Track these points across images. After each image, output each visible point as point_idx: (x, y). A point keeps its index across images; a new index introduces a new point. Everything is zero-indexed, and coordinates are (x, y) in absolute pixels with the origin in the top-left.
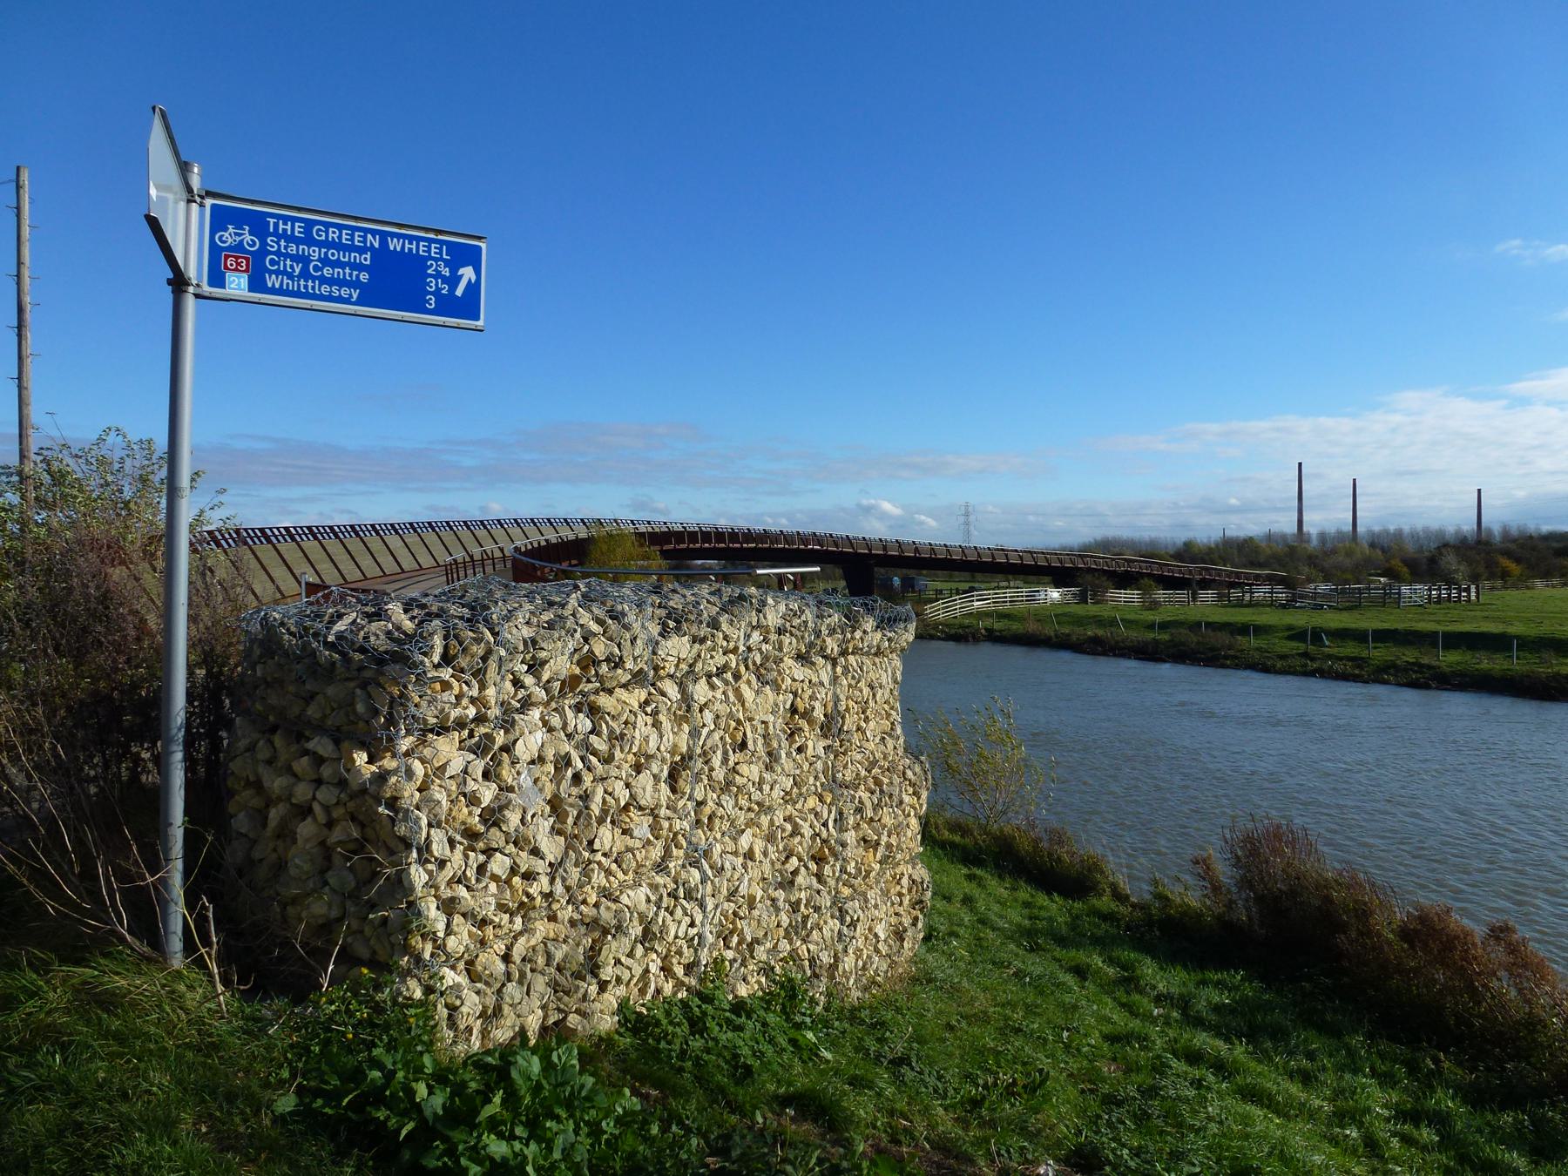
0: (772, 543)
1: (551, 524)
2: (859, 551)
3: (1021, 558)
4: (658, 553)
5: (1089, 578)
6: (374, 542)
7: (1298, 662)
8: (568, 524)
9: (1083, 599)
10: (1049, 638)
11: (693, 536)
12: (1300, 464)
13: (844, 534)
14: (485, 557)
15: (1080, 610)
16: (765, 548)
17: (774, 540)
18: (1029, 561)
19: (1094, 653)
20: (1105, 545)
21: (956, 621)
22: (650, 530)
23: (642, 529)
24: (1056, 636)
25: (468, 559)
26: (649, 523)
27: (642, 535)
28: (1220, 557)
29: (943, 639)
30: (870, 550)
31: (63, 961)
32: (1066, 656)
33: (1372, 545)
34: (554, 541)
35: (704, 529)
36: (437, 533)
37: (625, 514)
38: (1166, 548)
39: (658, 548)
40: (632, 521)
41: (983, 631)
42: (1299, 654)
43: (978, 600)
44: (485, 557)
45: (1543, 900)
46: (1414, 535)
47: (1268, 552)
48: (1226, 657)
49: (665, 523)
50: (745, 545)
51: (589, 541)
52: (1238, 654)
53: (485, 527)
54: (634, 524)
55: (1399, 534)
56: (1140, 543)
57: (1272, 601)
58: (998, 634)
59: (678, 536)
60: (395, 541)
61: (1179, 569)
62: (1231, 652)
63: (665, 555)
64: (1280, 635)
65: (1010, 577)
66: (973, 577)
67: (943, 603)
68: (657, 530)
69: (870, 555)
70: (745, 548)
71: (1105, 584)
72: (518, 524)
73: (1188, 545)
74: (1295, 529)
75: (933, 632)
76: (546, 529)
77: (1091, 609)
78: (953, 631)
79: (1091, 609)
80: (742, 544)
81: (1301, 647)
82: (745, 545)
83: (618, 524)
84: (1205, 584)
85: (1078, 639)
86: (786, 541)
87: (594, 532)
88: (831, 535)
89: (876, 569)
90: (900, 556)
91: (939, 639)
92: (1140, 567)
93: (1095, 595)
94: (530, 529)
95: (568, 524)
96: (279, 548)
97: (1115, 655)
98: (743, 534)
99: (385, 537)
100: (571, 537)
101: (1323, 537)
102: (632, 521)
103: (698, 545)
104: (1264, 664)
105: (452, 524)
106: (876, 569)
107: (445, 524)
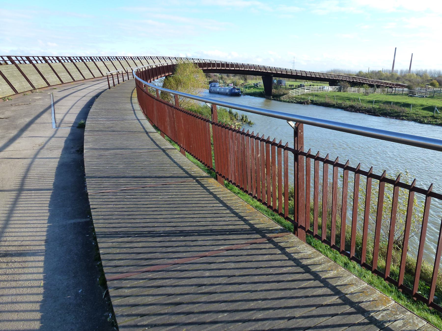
0: (245, 68)
2: (278, 72)
3: (306, 74)
5: (342, 83)
6: (91, 64)
7: (430, 119)
8: (170, 59)
9: (340, 90)
10: (334, 105)
12: (396, 48)
14: (118, 73)
15: (339, 94)
16: (247, 70)
17: (245, 67)
18: (304, 75)
19: (351, 111)
20: (334, 71)
21: (299, 97)
22: (199, 62)
23: (196, 62)
24: (337, 104)
25: (124, 72)
28: (370, 77)
29: (296, 103)
30: (282, 72)
32: (339, 111)
33: (417, 74)
36: (119, 61)
37: (190, 56)
38: (353, 72)
39: (202, 69)
40: (193, 59)
41: (310, 101)
42: (430, 116)
43: (306, 90)
46: (431, 72)
47: (385, 75)
48: (403, 116)
49: (204, 60)
50: (236, 69)
52: (407, 115)
53: (139, 59)
54: (193, 60)
55: (426, 71)
56: (345, 71)
57: (402, 93)
58: (315, 102)
59: (209, 64)
60: (100, 64)
61: (370, 80)
62: (404, 114)
64: (419, 108)
65: (308, 81)
66: (296, 80)
67: (295, 90)
68: (201, 62)
69: (272, 73)
70: (241, 70)
71: (348, 85)
73: (360, 72)
74: (391, 69)
75: (292, 100)
76: (150, 61)
77: (342, 94)
78: (299, 101)
79: (342, 94)
81: (431, 113)
82: (231, 68)
83: (193, 60)
84: (378, 86)
85: (345, 106)
86: (271, 70)
87: (179, 61)
88: (269, 67)
90: (286, 74)
91: (295, 103)
92: (343, 78)
93: (344, 89)
94: (144, 61)
95: (170, 59)
97: (360, 112)
98: (235, 65)
99: (135, 61)
100: (166, 65)
101: (402, 72)
104: (420, 120)
106: (273, 78)
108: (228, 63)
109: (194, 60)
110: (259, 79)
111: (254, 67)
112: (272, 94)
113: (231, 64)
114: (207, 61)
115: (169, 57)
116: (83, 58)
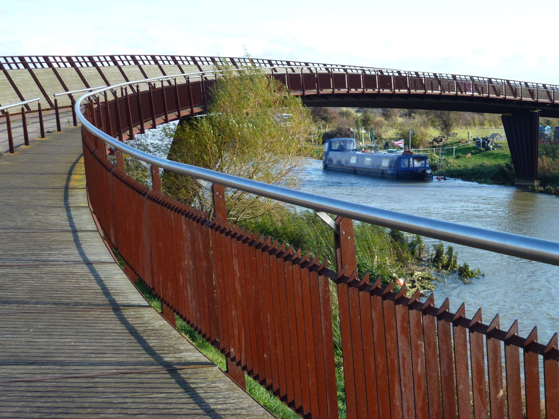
0: (443, 90)
1: (176, 62)
4: (299, 100)
11: (339, 80)
13: (524, 79)
14: (26, 110)
22: (290, 71)
23: (281, 71)
26: (288, 63)
27: (280, 77)
31: (355, 262)
34: (158, 85)
35: (368, 73)
39: (299, 93)
40: (270, 62)
44: (26, 110)
45: (112, 350)
49: (307, 64)
50: (413, 91)
51: (206, 84)
54: (272, 65)
63: (307, 101)
68: (298, 72)
69: (537, 104)
72: (136, 62)
80: (409, 89)
89: (541, 120)
96: (103, 71)
98: (411, 78)
100: (181, 81)
102: (270, 62)
103: (360, 90)
105: (51, 59)
107: (42, 60)
108: (386, 74)
109: (275, 66)
110: (493, 123)
111: (475, 84)
112: (540, 172)
113: (395, 77)
114: (318, 69)
115: (193, 58)
116: (74, 59)
